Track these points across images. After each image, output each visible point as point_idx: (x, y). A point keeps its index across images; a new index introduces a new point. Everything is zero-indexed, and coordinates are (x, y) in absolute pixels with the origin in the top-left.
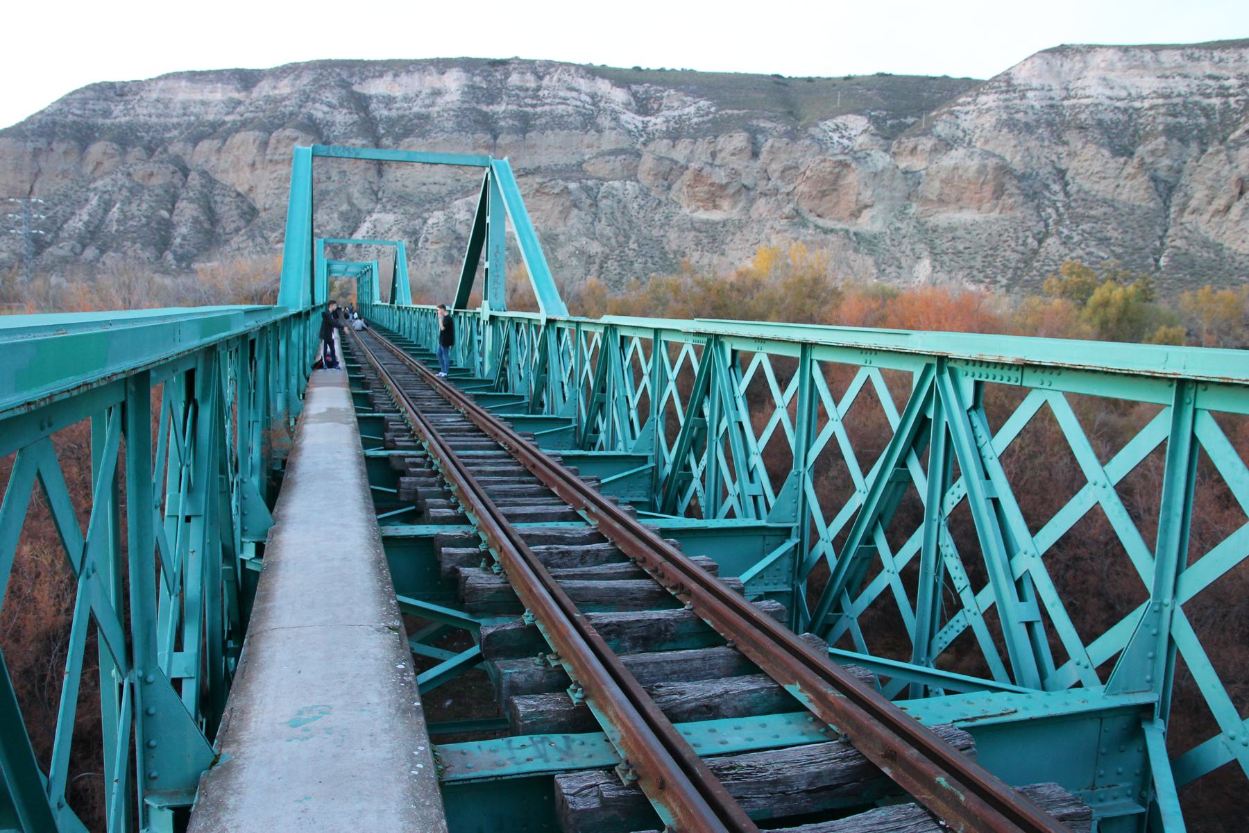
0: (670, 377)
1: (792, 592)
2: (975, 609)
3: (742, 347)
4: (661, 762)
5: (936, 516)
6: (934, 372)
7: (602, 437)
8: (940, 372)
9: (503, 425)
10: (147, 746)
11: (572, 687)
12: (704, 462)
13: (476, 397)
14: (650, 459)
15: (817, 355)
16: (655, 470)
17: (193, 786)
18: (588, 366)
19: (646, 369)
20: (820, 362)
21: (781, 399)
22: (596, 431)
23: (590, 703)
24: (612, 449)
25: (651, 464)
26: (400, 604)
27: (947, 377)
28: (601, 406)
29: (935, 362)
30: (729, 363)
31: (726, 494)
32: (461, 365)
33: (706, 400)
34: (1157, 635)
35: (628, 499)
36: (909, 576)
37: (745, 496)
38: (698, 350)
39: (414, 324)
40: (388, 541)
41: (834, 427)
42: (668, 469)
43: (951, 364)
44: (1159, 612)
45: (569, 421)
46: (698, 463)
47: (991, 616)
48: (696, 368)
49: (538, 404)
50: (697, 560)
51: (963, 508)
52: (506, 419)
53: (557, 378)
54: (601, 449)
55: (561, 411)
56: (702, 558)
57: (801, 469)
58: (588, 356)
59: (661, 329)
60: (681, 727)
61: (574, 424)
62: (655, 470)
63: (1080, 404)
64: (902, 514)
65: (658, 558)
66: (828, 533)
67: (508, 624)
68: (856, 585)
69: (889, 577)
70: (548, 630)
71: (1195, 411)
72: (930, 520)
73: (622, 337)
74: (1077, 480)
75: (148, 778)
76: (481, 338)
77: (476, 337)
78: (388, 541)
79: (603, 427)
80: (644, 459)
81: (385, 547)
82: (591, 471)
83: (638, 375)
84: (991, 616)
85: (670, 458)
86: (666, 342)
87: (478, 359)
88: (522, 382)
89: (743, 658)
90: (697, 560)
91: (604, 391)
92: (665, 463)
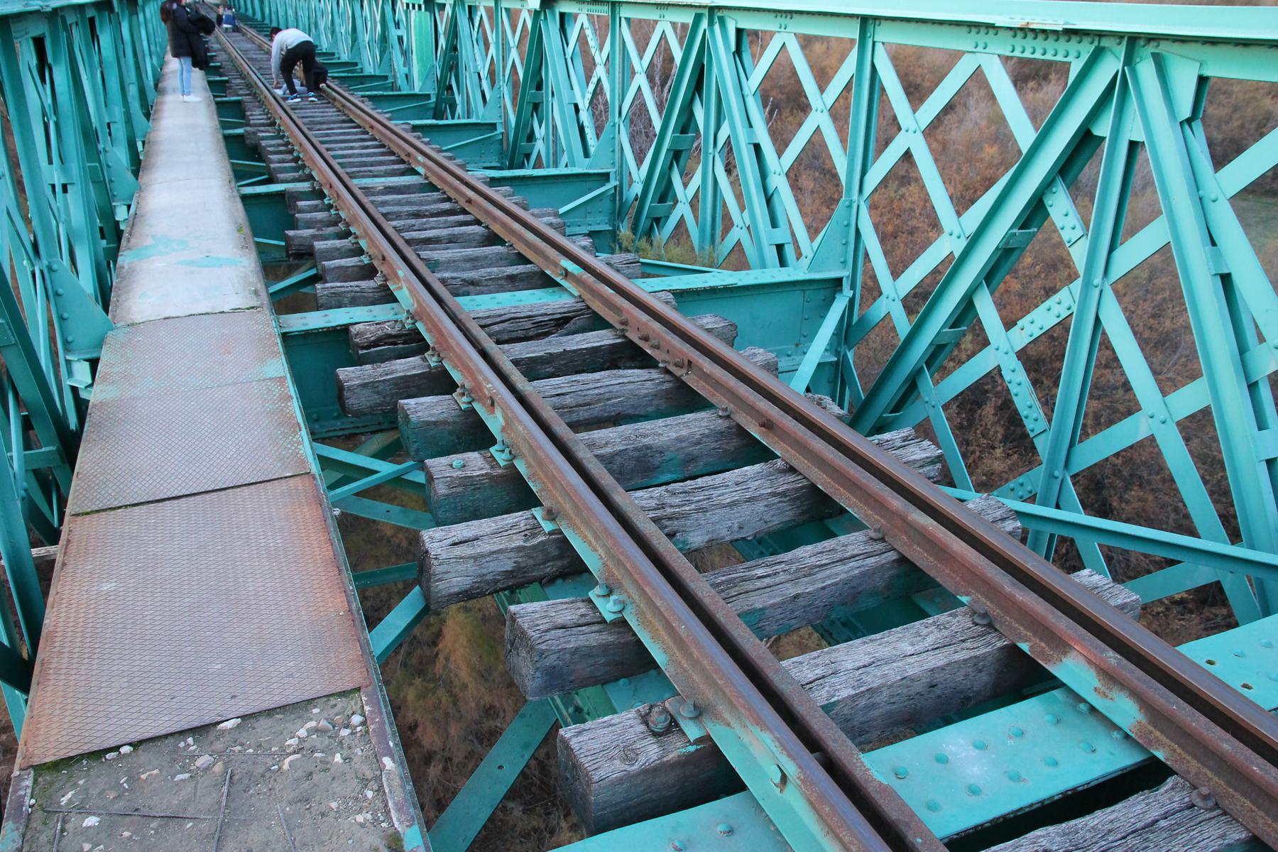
0: (637, 68)
1: (837, 362)
2: (893, 295)
3: (748, 23)
4: (458, 344)
5: (711, 150)
6: (704, 24)
7: (539, 146)
8: (711, 24)
9: (368, 106)
10: (62, 319)
11: (459, 390)
12: (696, 181)
13: (371, 98)
14: (612, 177)
15: (883, 35)
16: (619, 190)
17: (100, 344)
18: (514, 55)
19: (600, 58)
20: (628, 20)
21: (820, 102)
22: (531, 137)
23: (516, 463)
24: (556, 165)
25: (613, 182)
26: (257, 244)
27: (717, 27)
28: (536, 107)
29: (706, 12)
30: (733, 48)
31: (728, 224)
32: (369, 70)
33: (697, 101)
34: (848, 225)
35: (585, 230)
36: (1042, 363)
37: (775, 238)
38: (681, 30)
39: (290, 12)
40: (245, 198)
41: (911, 136)
42: (637, 189)
43: (720, 14)
44: (850, 207)
45: (493, 126)
46: (685, 185)
47: (1199, 428)
48: (678, 55)
49: (444, 102)
50: (703, 323)
51: (1163, 264)
52: (415, 128)
53: (566, 100)
54: (538, 164)
55: (481, 115)
56: (709, 320)
57: (855, 197)
58: (513, 41)
59: (877, 19)
60: (461, 300)
61: (391, 80)
62: (619, 190)
63: (806, 42)
64: (1025, 266)
65: (644, 317)
66: (895, 291)
67: (474, 463)
68: (942, 357)
69: (1002, 350)
70: (429, 331)
71: (874, 43)
72: (707, 153)
73: (562, 15)
74: (931, 132)
75: (66, 343)
76: (402, 32)
77: (394, 33)
78: (245, 198)
79: (539, 132)
80: (605, 177)
81: (244, 205)
82: (531, 194)
83: (590, 67)
84: (1199, 428)
85: (639, 174)
86: (628, 20)
87: (398, 59)
88: (486, 101)
89: (682, 387)
90: (703, 323)
91: (539, 87)
92: (631, 182)
